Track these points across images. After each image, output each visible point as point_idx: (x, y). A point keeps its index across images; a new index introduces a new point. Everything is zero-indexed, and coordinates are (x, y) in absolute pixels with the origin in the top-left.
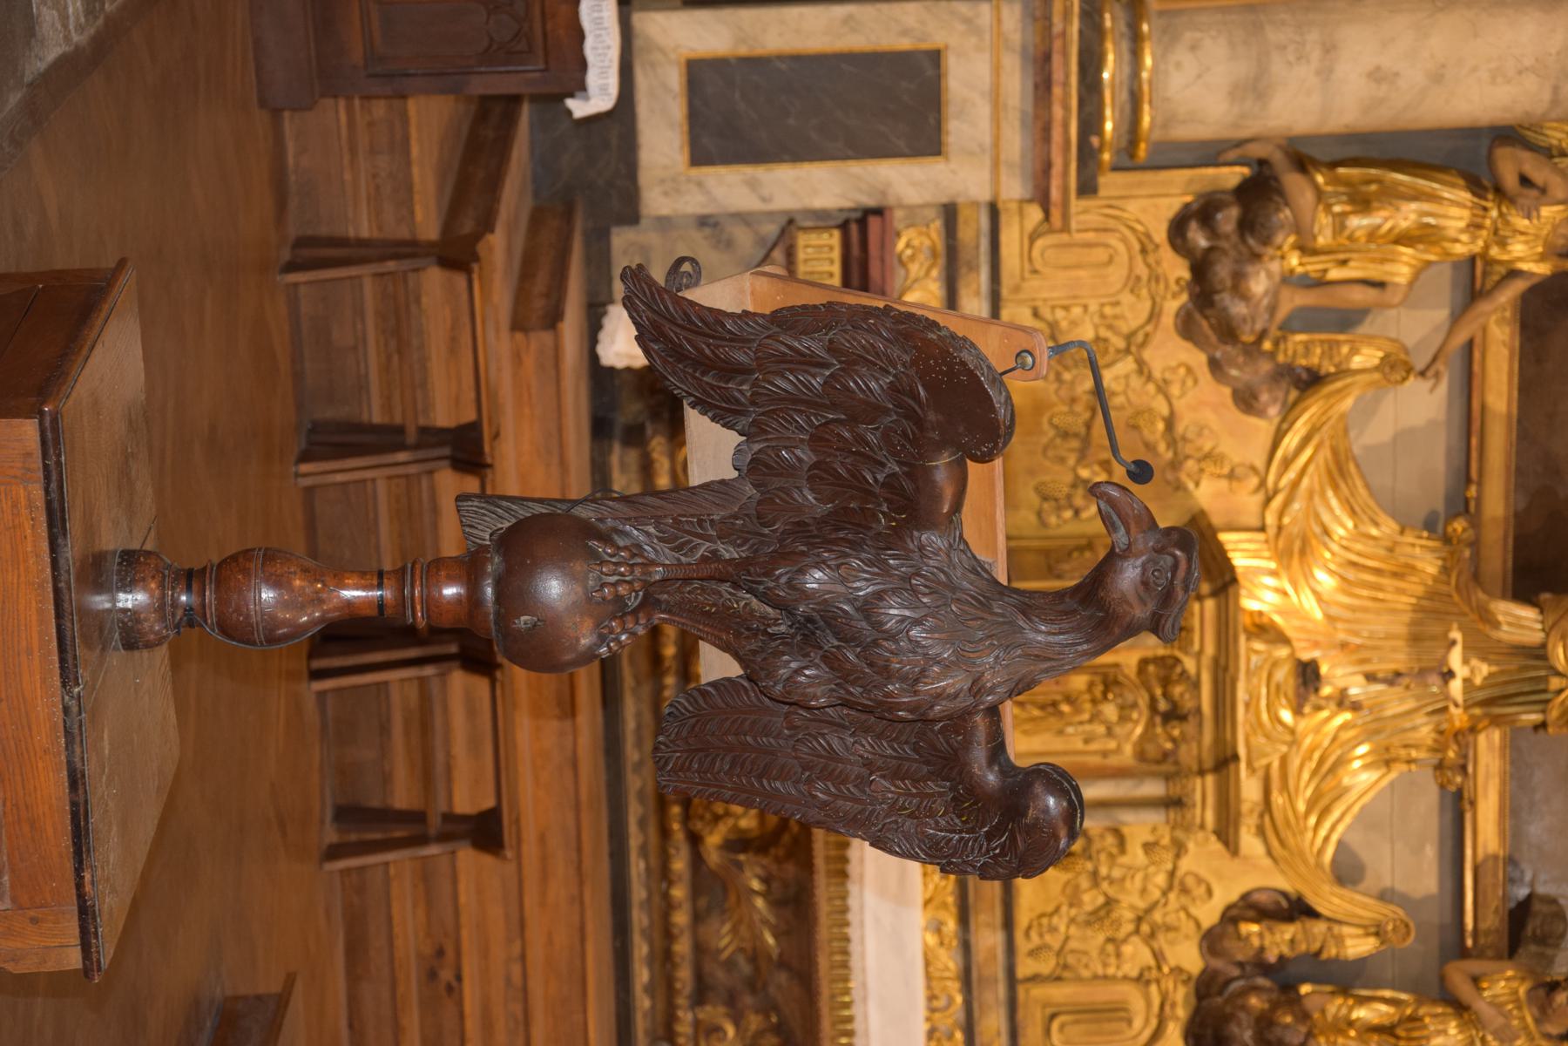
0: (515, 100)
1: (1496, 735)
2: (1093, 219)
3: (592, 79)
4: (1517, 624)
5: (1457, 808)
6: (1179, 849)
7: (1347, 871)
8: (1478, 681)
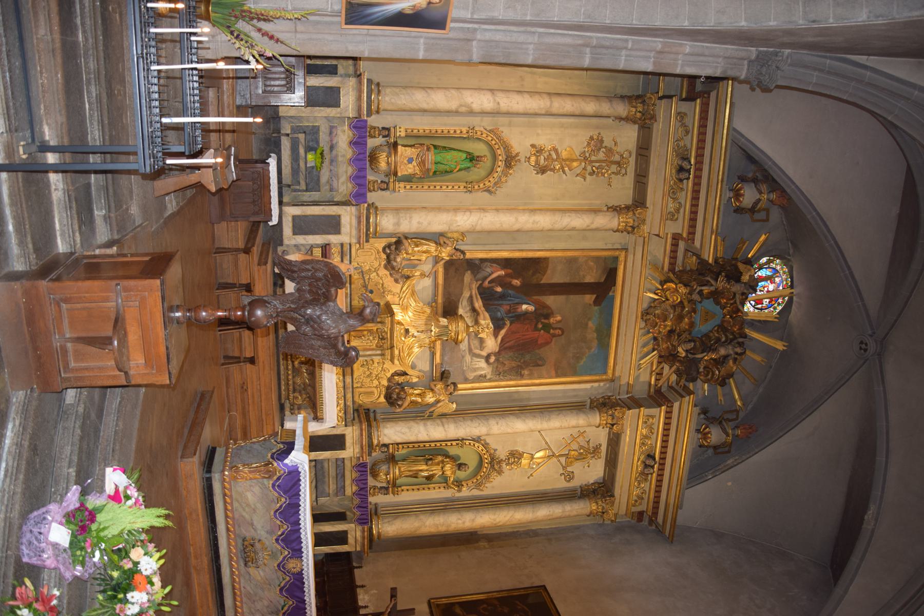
0: (260, 222)
1: (439, 342)
2: (369, 247)
3: (273, 218)
4: (443, 322)
5: (433, 355)
6: (384, 363)
7: (413, 367)
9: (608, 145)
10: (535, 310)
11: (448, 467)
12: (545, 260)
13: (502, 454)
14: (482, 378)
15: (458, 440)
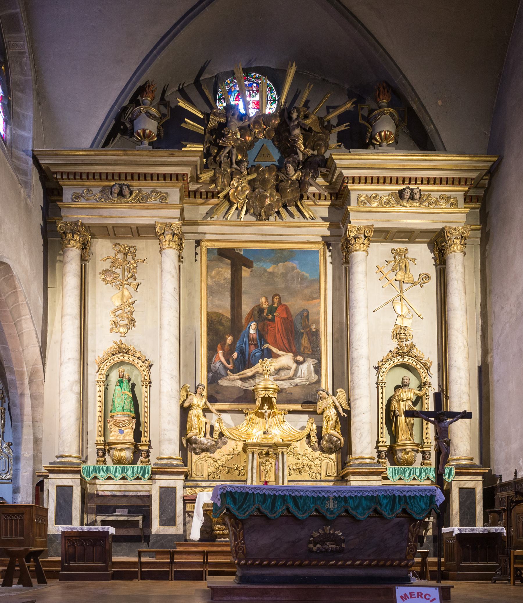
8: (267, 407)
9: (110, 264)
10: (255, 321)
11: (404, 396)
12: (209, 314)
13: (393, 345)
14: (318, 370)
15: (377, 387)
